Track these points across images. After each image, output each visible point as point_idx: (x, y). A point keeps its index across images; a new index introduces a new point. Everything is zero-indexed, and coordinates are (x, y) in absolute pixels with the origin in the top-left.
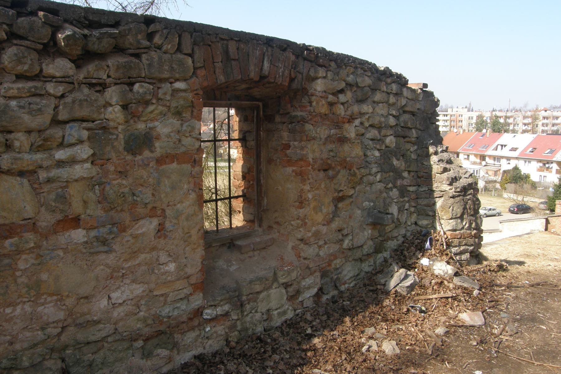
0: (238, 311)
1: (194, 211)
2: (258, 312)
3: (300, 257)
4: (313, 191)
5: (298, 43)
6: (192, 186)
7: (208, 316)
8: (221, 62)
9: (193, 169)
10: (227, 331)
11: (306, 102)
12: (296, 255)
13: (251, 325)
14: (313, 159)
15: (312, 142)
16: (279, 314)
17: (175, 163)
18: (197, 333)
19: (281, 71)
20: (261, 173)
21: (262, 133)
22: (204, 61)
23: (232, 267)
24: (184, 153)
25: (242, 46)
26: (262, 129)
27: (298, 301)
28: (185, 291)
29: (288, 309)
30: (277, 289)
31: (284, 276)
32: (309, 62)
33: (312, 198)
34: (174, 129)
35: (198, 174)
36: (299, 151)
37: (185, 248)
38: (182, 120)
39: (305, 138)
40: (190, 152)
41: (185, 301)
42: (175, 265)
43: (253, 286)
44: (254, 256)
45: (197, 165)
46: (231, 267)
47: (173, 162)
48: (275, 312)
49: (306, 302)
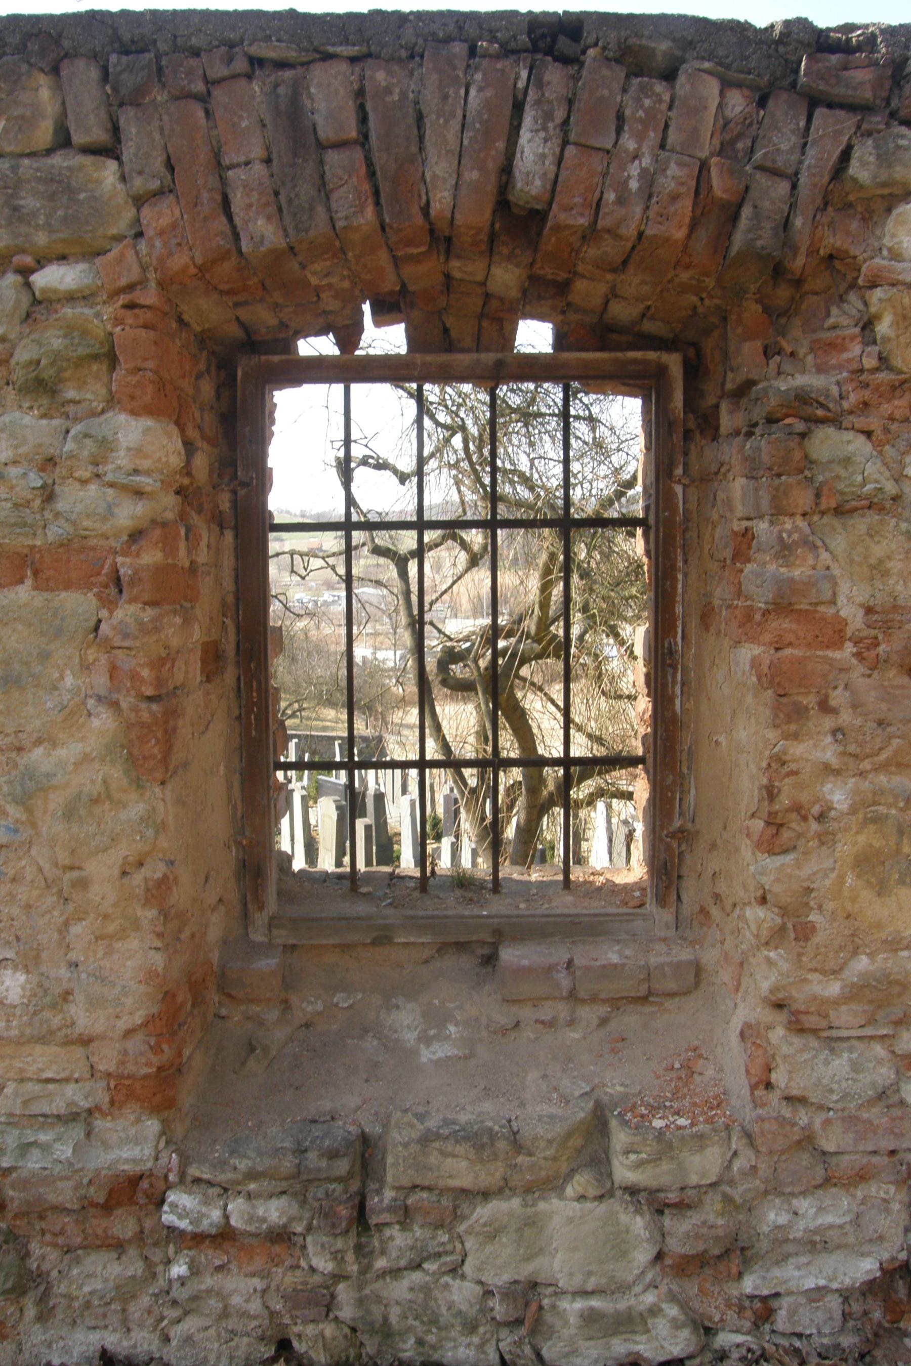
0: (339, 1244)
1: (105, 782)
2: (463, 1277)
3: (769, 1085)
4: (862, 774)
5: (760, 22)
6: (101, 681)
7: (180, 1217)
8: (268, 161)
9: (104, 613)
10: (277, 1305)
11: (844, 320)
12: (748, 1072)
13: (411, 1321)
14: (869, 611)
15: (861, 524)
16: (590, 1318)
17: (29, 582)
18: (134, 1267)
19: (634, 170)
20: (674, 667)
21: (679, 489)
22: (170, 166)
23: (435, 1046)
24: (61, 545)
25: (381, 76)
26: (679, 471)
27: (734, 1291)
28: (70, 1090)
29: (654, 1311)
30: (589, 1205)
31: (633, 1157)
32: (841, 114)
33: (853, 811)
34: (20, 451)
35: (126, 636)
36: (772, 567)
37: (66, 924)
38: (67, 417)
39: (803, 499)
40: (93, 542)
41: (77, 1132)
42: (27, 981)
43: (433, 1159)
44: (571, 1023)
45: (125, 596)
46: (428, 1046)
47: (21, 581)
48: (573, 1307)
49: (792, 1313)
